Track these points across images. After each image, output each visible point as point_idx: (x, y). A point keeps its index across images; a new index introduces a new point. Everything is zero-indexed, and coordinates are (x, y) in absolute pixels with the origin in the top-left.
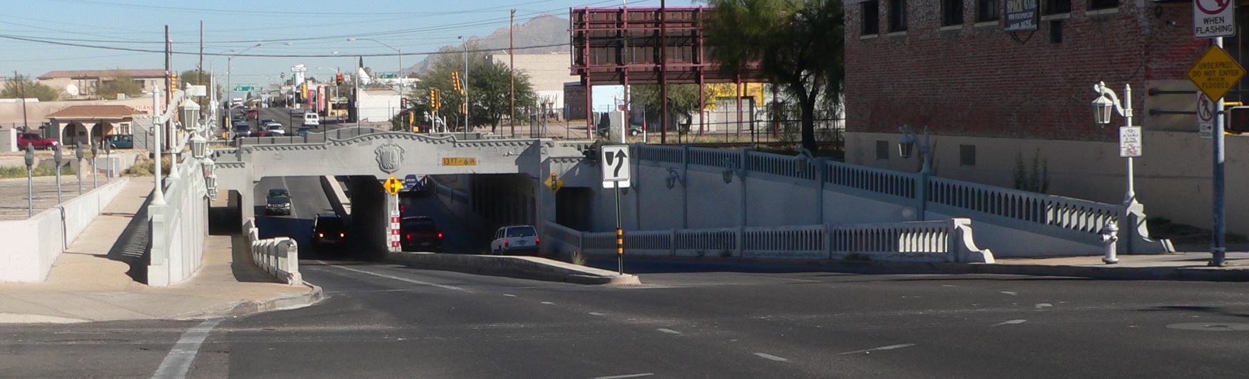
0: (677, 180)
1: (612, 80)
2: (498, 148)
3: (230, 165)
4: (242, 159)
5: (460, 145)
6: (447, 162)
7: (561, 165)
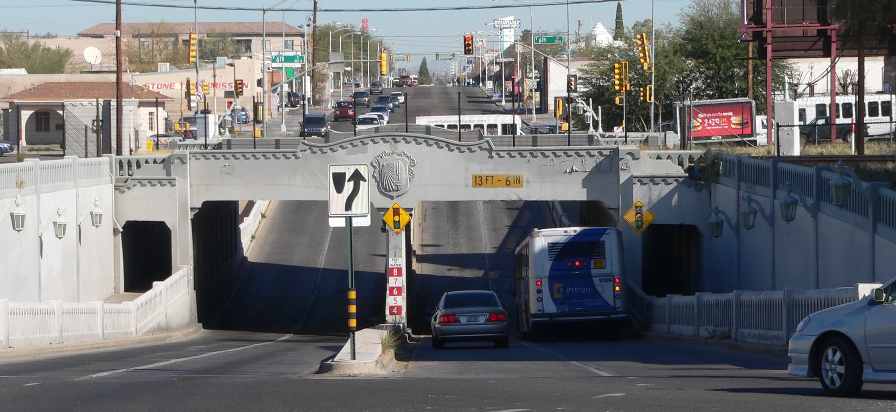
0: (759, 215)
1: (810, 49)
2: (556, 160)
3: (154, 182)
4: (172, 173)
5: (498, 154)
6: (478, 181)
7: (650, 189)
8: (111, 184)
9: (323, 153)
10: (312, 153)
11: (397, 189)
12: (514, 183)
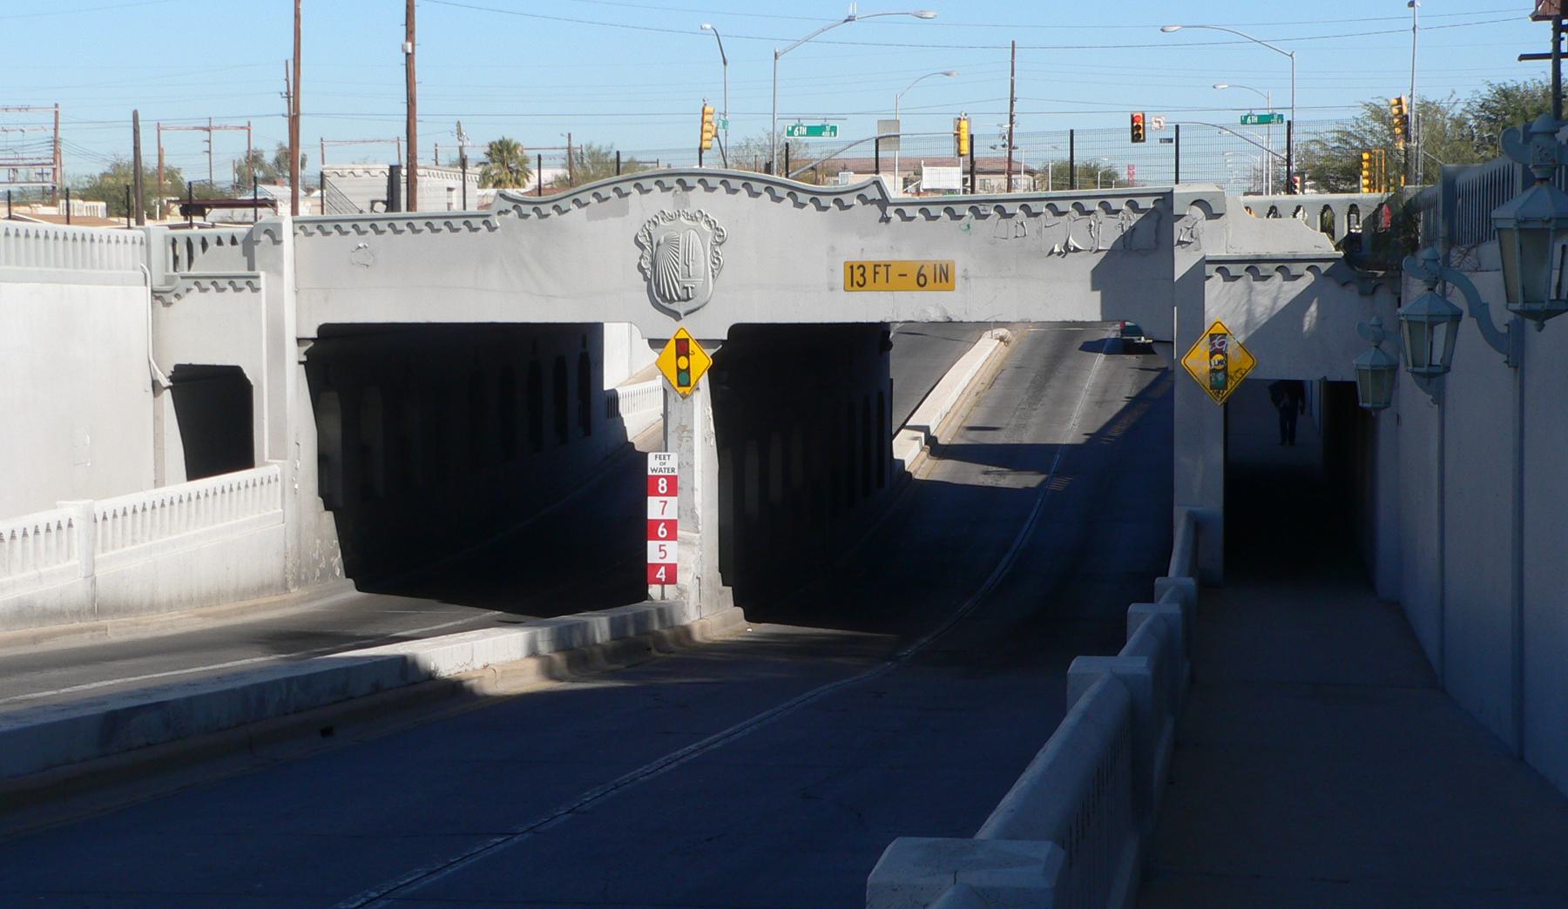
0: (1468, 325)
6: (858, 278)
8: (145, 287)
9: (542, 216)
10: (520, 217)
11: (686, 297)
12: (935, 281)
